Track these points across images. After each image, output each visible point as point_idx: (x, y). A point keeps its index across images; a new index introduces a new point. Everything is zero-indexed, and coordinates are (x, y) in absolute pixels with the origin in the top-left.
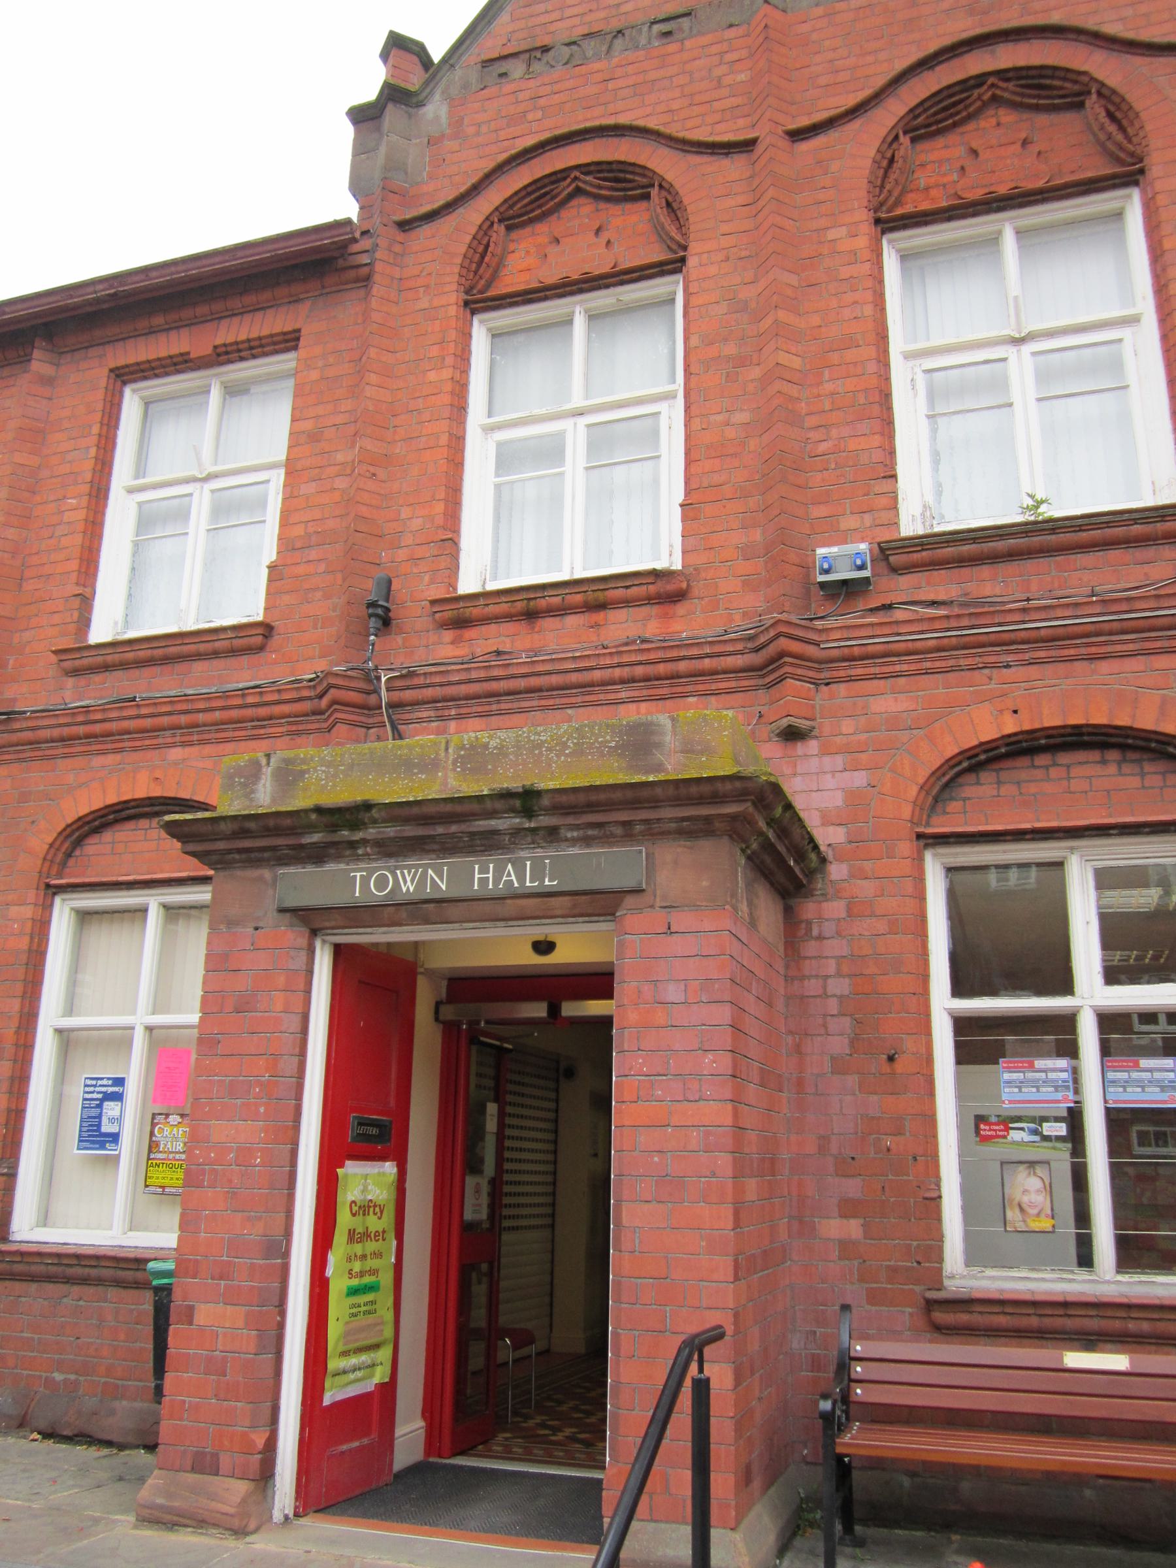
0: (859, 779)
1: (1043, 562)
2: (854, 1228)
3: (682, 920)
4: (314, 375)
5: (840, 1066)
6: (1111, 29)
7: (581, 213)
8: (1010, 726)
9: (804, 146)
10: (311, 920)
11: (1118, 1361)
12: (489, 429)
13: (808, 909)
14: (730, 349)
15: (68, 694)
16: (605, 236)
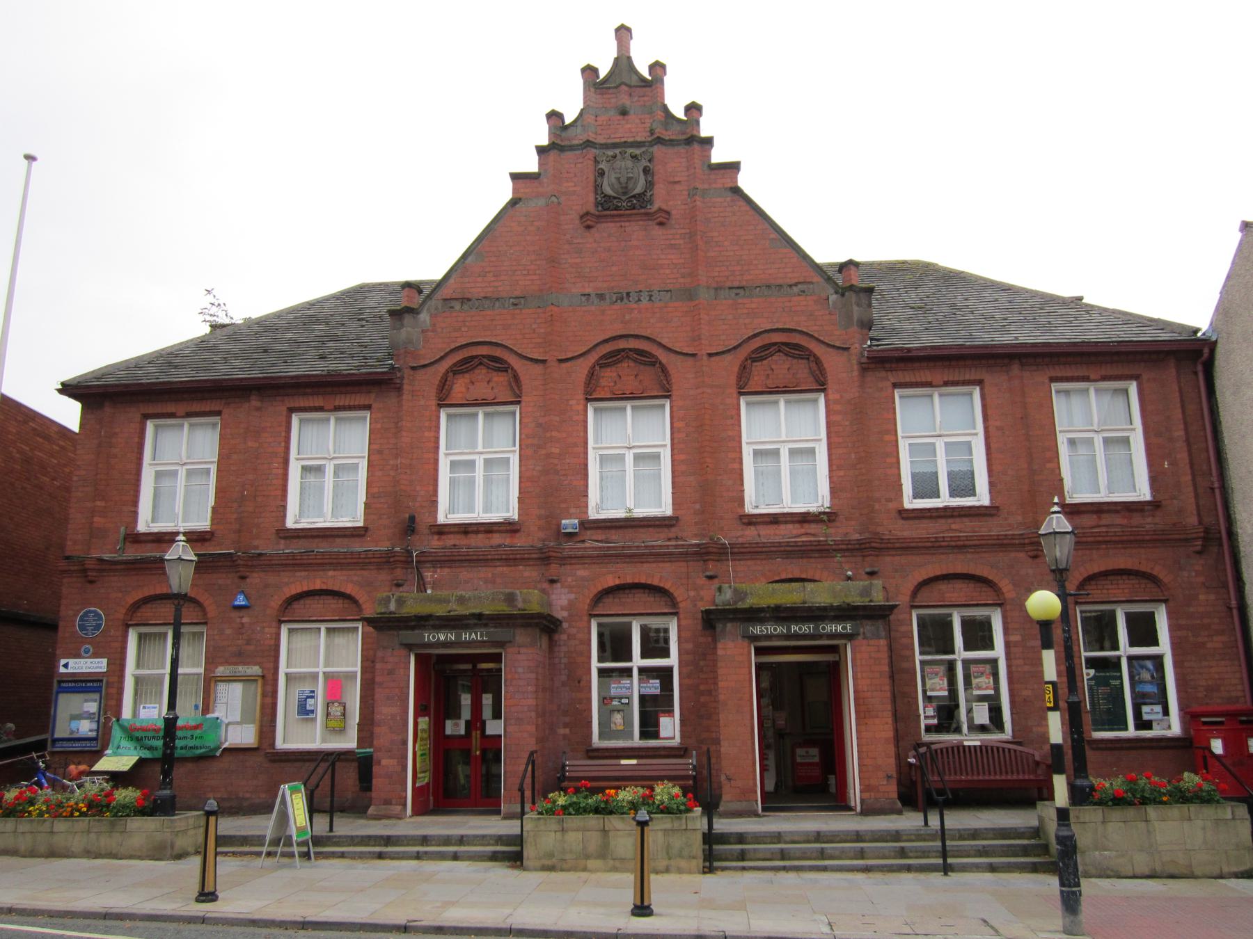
0: (572, 596)
1: (630, 530)
2: (567, 731)
3: (523, 650)
4: (379, 426)
5: (564, 684)
6: (664, 342)
7: (481, 372)
8: (617, 582)
9: (563, 365)
10: (409, 647)
11: (634, 762)
12: (447, 455)
13: (556, 637)
14: (535, 441)
15: (282, 546)
16: (491, 384)
